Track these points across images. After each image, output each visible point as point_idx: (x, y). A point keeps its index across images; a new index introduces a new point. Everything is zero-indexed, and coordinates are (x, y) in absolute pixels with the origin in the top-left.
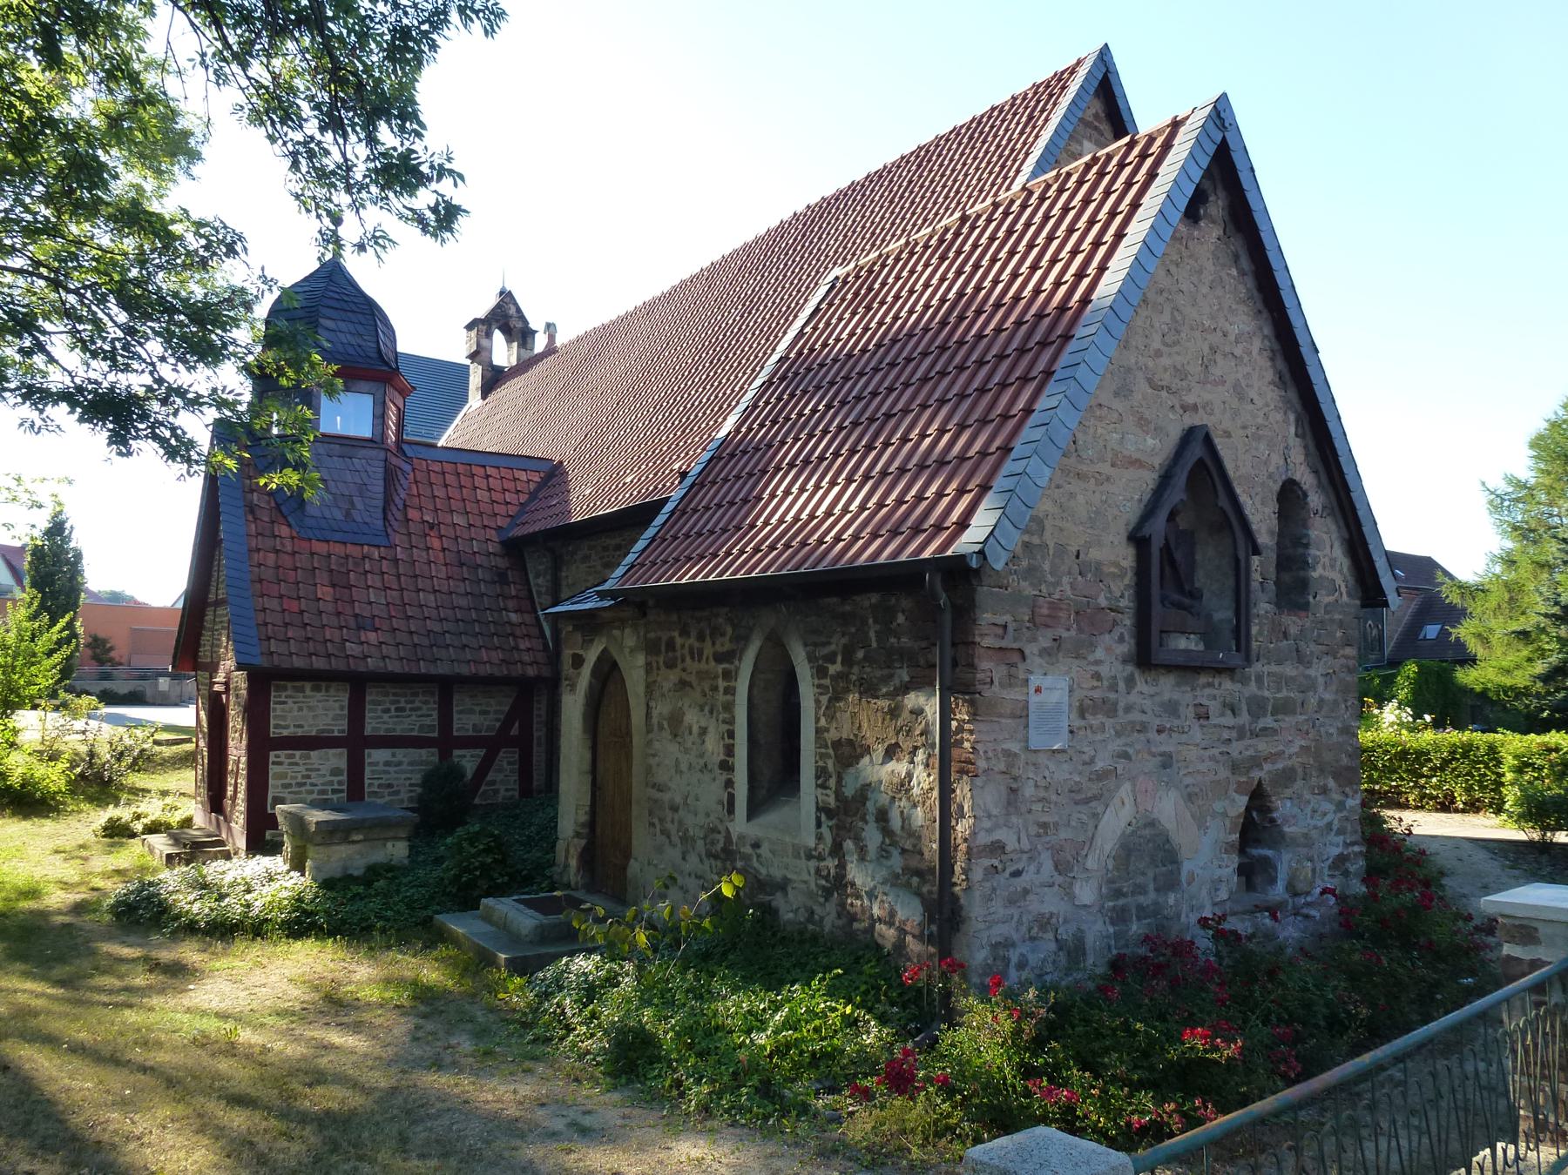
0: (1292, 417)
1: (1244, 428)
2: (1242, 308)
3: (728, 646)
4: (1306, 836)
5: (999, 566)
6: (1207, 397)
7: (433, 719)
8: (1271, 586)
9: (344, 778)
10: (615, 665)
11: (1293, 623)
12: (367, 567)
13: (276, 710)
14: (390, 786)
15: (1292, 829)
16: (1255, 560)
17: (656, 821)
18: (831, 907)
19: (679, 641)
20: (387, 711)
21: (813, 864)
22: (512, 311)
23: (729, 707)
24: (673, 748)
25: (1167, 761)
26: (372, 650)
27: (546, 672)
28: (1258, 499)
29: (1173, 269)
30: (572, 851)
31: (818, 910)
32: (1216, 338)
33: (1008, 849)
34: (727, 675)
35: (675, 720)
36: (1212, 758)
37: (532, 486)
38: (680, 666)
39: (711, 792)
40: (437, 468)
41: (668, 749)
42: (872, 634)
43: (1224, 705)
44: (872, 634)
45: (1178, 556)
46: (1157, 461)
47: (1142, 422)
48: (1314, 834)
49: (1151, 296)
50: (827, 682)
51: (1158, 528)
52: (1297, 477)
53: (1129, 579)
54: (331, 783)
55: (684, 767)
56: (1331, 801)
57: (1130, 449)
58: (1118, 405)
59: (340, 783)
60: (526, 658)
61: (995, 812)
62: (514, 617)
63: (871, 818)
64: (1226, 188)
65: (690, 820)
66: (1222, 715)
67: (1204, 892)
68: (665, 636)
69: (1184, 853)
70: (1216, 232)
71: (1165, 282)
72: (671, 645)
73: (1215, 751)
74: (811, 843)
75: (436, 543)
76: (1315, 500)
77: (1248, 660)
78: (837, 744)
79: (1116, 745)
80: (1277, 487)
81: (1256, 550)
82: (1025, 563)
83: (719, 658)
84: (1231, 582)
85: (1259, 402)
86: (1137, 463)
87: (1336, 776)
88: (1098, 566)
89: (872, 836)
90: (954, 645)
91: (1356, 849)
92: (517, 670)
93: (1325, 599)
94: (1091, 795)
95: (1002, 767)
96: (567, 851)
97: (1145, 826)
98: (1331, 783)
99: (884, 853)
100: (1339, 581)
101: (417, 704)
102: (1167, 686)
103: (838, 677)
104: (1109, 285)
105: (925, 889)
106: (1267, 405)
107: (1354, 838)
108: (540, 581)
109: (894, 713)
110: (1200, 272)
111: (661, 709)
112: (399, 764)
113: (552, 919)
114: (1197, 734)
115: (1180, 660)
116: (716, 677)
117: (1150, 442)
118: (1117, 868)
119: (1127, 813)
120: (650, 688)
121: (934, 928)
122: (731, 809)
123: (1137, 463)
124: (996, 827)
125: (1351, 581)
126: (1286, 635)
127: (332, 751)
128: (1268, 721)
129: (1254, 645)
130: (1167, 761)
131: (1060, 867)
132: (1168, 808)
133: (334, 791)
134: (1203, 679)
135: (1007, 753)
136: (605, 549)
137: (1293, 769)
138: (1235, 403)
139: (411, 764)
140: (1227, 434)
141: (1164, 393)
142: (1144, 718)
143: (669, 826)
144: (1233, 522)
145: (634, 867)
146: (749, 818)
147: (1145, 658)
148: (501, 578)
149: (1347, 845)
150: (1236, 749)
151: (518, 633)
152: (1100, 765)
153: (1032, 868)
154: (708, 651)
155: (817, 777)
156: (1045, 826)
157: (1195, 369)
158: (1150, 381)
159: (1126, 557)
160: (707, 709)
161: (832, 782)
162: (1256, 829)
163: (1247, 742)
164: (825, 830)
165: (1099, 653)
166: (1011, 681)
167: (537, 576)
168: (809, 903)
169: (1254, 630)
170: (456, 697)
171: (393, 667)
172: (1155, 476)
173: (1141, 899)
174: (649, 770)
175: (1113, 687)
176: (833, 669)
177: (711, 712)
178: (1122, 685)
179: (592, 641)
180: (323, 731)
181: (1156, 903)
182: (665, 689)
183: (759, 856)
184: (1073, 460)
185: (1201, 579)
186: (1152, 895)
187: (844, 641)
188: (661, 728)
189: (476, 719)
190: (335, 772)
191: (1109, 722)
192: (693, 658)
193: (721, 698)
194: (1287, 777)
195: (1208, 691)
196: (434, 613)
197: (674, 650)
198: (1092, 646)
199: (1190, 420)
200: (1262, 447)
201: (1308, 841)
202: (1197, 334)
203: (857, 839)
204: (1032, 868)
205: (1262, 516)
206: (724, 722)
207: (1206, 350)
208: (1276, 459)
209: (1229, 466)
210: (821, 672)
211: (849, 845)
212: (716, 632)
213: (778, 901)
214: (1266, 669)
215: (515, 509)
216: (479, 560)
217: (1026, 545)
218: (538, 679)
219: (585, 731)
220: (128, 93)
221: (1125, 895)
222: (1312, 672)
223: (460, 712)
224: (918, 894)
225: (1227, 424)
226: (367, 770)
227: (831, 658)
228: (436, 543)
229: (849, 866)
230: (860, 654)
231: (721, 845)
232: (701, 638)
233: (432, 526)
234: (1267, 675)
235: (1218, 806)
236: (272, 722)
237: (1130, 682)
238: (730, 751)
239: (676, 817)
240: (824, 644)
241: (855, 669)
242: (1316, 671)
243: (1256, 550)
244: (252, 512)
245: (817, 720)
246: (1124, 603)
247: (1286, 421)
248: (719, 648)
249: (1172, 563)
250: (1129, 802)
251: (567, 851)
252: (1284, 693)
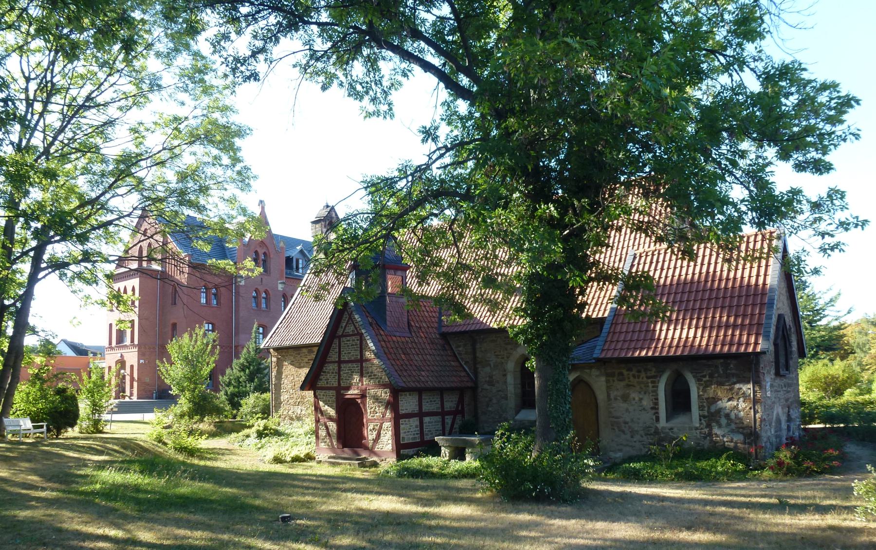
3: (653, 373)
22: (334, 215)
24: (625, 405)
72: (621, 374)
78: (707, 399)
89: (724, 421)
99: (728, 425)
104: (298, 522)
108: (460, 349)
109: (731, 389)
120: (609, 388)
122: (658, 419)
220: (117, 47)
227: (705, 376)
238: (656, 404)
248: (649, 374)
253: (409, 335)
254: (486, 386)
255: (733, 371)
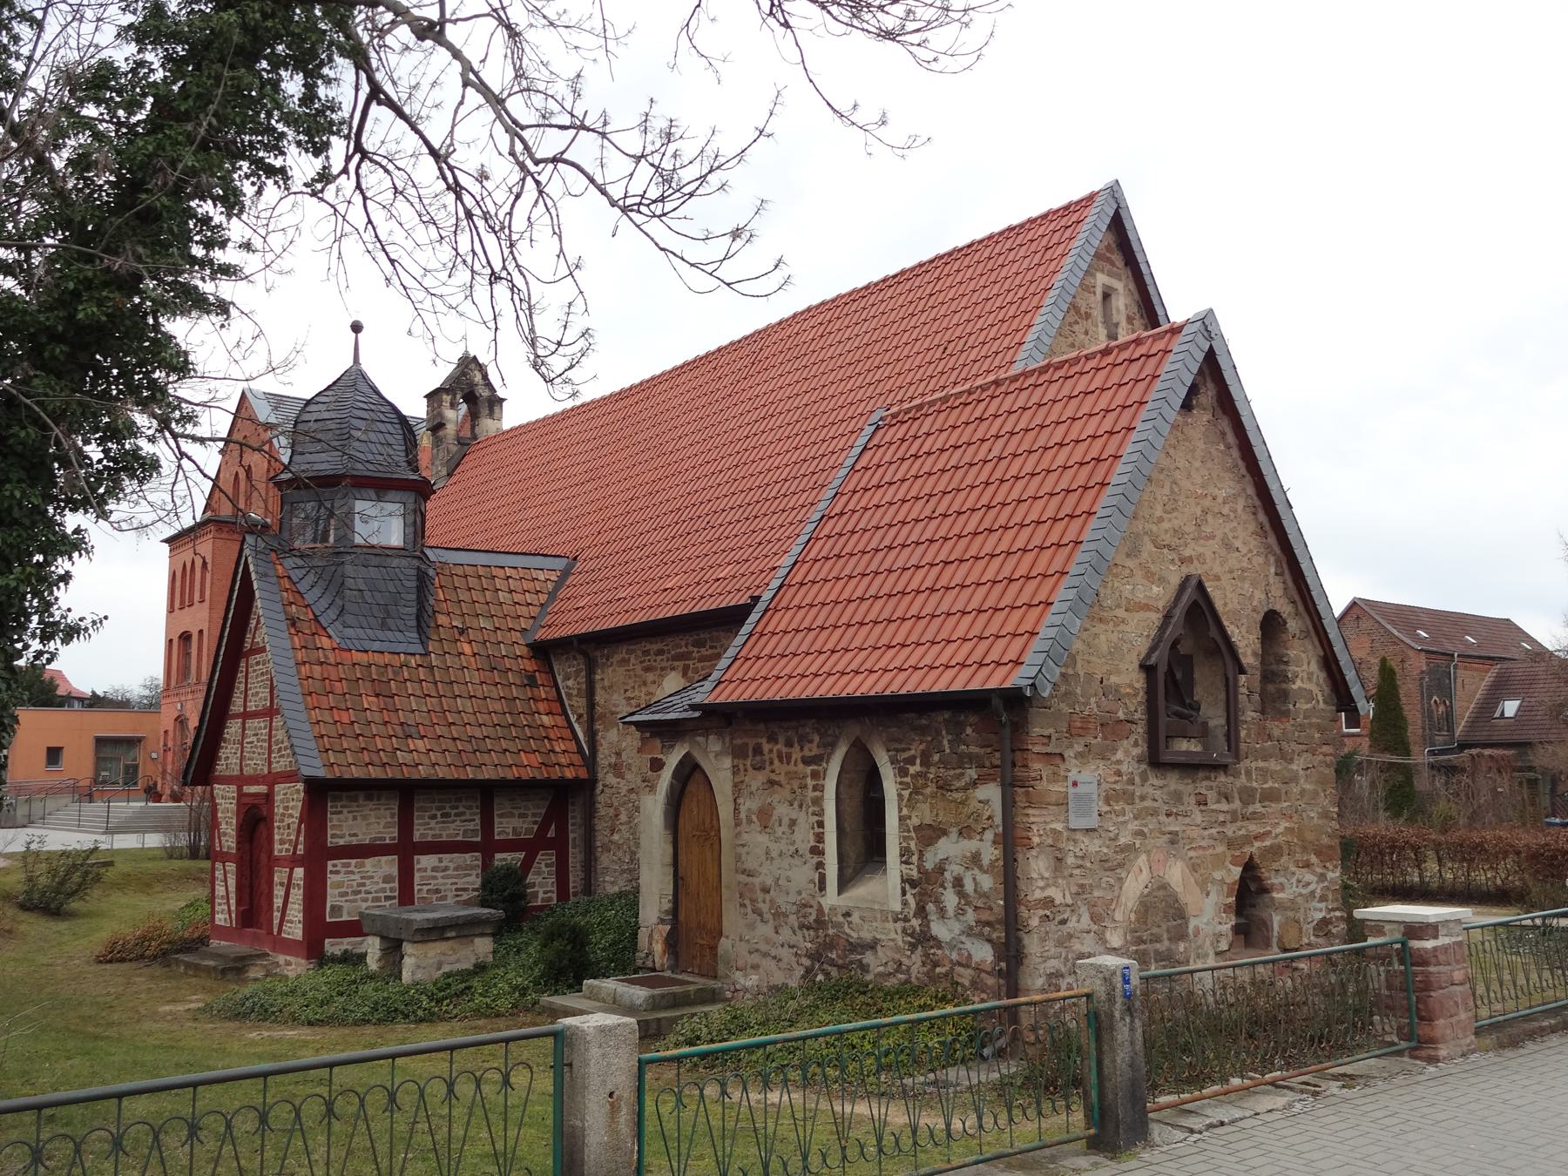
0: (1272, 559)
1: (1231, 572)
2: (1228, 475)
3: (815, 751)
4: (1292, 901)
5: (1045, 694)
6: (1201, 550)
7: (476, 824)
8: (1256, 697)
9: (396, 885)
10: (696, 767)
11: (1276, 728)
12: (406, 675)
13: (333, 820)
14: (437, 891)
15: (1281, 895)
16: (1243, 678)
17: (747, 902)
18: (917, 957)
19: (766, 747)
20: (434, 817)
21: (899, 925)
23: (818, 802)
24: (763, 839)
25: (1174, 839)
26: (424, 759)
27: (583, 774)
28: (1244, 630)
29: (1172, 451)
30: (656, 936)
31: (905, 961)
32: (1207, 502)
33: (1057, 902)
34: (815, 775)
35: (765, 815)
36: (1211, 837)
37: (550, 586)
38: (768, 768)
39: (802, 874)
40: (459, 571)
41: (757, 839)
42: (945, 742)
43: (1219, 793)
44: (945, 742)
45: (1179, 676)
46: (1160, 605)
47: (1149, 575)
48: (1300, 900)
49: (1155, 475)
50: (908, 779)
51: (1160, 658)
52: (1277, 608)
53: (1141, 697)
54: (384, 890)
55: (774, 854)
56: (1314, 873)
57: (1140, 596)
58: (1130, 563)
59: (392, 890)
60: (563, 760)
61: (1047, 875)
62: (546, 720)
63: (949, 885)
64: (1213, 381)
65: (781, 900)
66: (1218, 802)
67: (1208, 943)
68: (752, 743)
69: (1191, 910)
70: (1206, 417)
71: (1165, 462)
72: (758, 750)
73: (1213, 831)
74: (897, 907)
75: (467, 649)
76: (1293, 625)
77: (1237, 757)
79: (1134, 826)
80: (1260, 617)
81: (1242, 671)
82: (1063, 689)
83: (807, 761)
84: (1223, 696)
85: (1244, 550)
86: (1146, 607)
87: (1318, 854)
88: (1117, 688)
90: (1013, 751)
91: (1338, 914)
92: (556, 773)
93: (1303, 706)
94: (1116, 863)
95: (1050, 841)
96: (651, 936)
97: (1159, 888)
98: (1313, 859)
99: (960, 912)
100: (1316, 690)
101: (461, 809)
102: (1173, 782)
103: (918, 775)
105: (994, 936)
106: (1250, 551)
107: (1335, 905)
108: (570, 683)
110: (1193, 451)
111: (749, 805)
112: (446, 869)
113: (657, 991)
114: (1198, 817)
115: (1182, 759)
116: (804, 777)
117: (1155, 589)
118: (1138, 920)
119: (1145, 876)
120: (737, 787)
121: (1003, 965)
123: (1146, 607)
124: (1048, 886)
125: (1327, 690)
126: (1270, 737)
127: (384, 859)
128: (1258, 807)
129: (1243, 746)
130: (1174, 839)
131: (1095, 918)
132: (1176, 874)
133: (387, 898)
134: (1201, 775)
135: (1054, 831)
136: (647, 653)
137: (1280, 847)
138: (1223, 552)
139: (456, 869)
140: (1217, 578)
141: (1166, 551)
142: (1156, 805)
143: (761, 905)
144: (1224, 649)
145: (724, 944)
146: (839, 893)
147: (1156, 761)
148: (531, 682)
149: (1330, 910)
150: (1230, 830)
151: (552, 736)
152: (1122, 841)
153: (1074, 918)
154: (796, 754)
155: (902, 856)
156: (1082, 886)
157: (1190, 528)
158: (1153, 542)
159: (1138, 681)
160: (796, 804)
161: (915, 859)
162: (1249, 894)
163: (1239, 824)
164: (909, 897)
165: (1120, 755)
166: (1055, 777)
167: (567, 678)
168: (897, 957)
169: (1243, 734)
170: (496, 801)
171: (442, 773)
172: (1160, 615)
173: (1158, 946)
174: (738, 858)
175: (1131, 782)
176: (914, 769)
177: (801, 806)
178: (1137, 779)
179: (672, 747)
180: (375, 839)
181: (1169, 950)
182: (754, 788)
183: (850, 923)
184: (1096, 608)
185: (1199, 693)
186: (1166, 943)
187: (922, 747)
188: (750, 821)
189: (516, 822)
190: (387, 879)
191: (1128, 808)
192: (781, 761)
193: (811, 794)
194: (1275, 852)
195: (1205, 783)
196: (472, 719)
197: (762, 754)
198: (1114, 751)
199: (1185, 570)
200: (1247, 586)
201: (1292, 905)
202: (1191, 501)
203: (937, 902)
204: (1074, 918)
205: (1246, 640)
206: (814, 814)
207: (1199, 513)
208: (1259, 595)
209: (1218, 605)
210: (903, 772)
211: (931, 907)
212: (804, 740)
213: (868, 958)
214: (1254, 765)
215: (537, 609)
216: (508, 663)
217: (1063, 675)
218: (576, 780)
219: (666, 827)
221: (1144, 942)
222: (1294, 767)
223: (501, 816)
224: (989, 941)
225: (1217, 569)
226: (417, 875)
227: (911, 761)
228: (467, 649)
229: (932, 925)
230: (936, 757)
231: (812, 918)
232: (789, 744)
233: (462, 631)
234: (1252, 771)
235: (1217, 875)
236: (330, 832)
237: (1144, 779)
238: (820, 838)
239: (768, 897)
240: (904, 750)
241: (933, 770)
242: (1297, 766)
243: (1242, 671)
244: (293, 625)
245: (900, 810)
246: (1137, 716)
247: (1267, 563)
248: (807, 753)
249: (1175, 682)
250: (1146, 871)
251: (651, 936)
252: (1269, 784)
253: (419, 649)
254: (611, 779)
255: (974, 749)
